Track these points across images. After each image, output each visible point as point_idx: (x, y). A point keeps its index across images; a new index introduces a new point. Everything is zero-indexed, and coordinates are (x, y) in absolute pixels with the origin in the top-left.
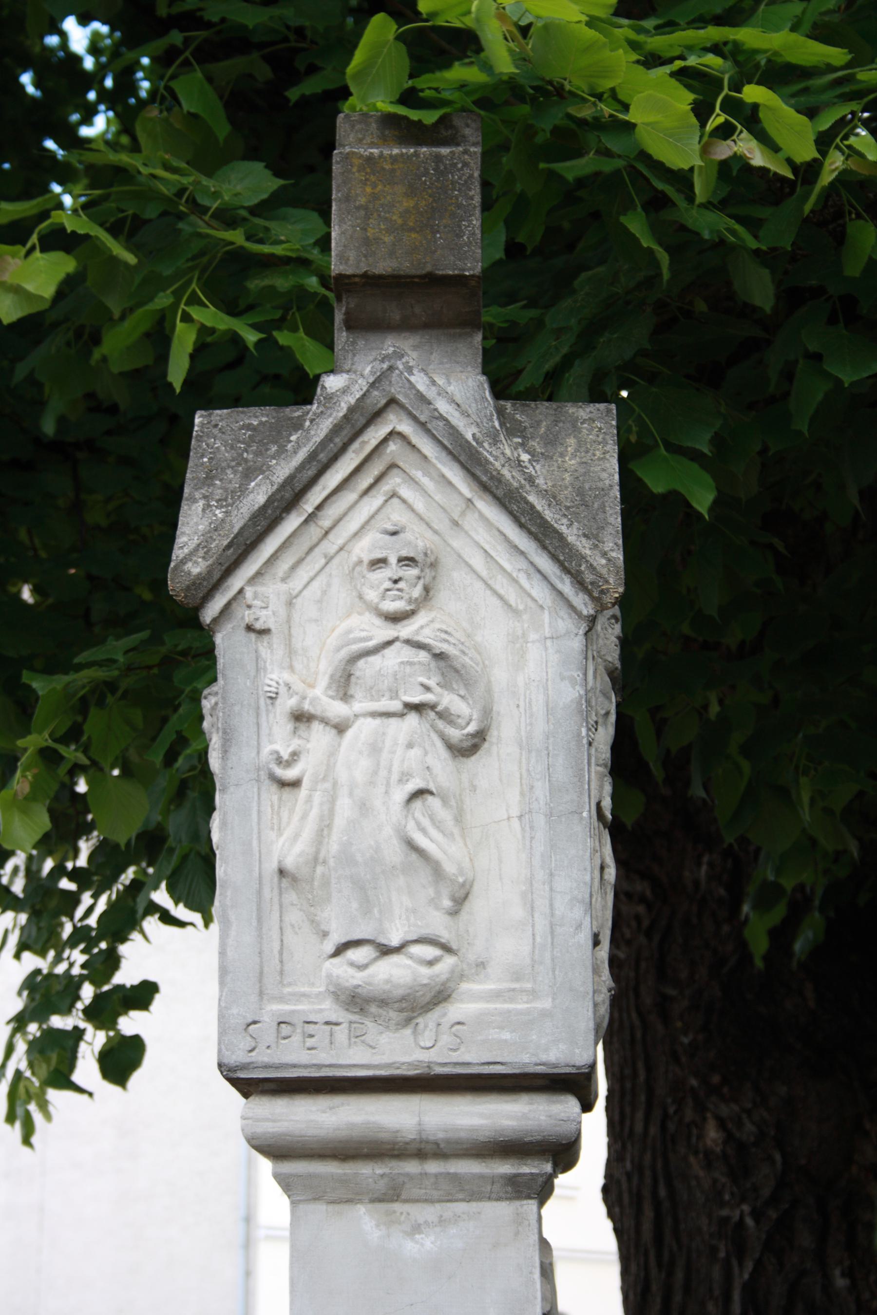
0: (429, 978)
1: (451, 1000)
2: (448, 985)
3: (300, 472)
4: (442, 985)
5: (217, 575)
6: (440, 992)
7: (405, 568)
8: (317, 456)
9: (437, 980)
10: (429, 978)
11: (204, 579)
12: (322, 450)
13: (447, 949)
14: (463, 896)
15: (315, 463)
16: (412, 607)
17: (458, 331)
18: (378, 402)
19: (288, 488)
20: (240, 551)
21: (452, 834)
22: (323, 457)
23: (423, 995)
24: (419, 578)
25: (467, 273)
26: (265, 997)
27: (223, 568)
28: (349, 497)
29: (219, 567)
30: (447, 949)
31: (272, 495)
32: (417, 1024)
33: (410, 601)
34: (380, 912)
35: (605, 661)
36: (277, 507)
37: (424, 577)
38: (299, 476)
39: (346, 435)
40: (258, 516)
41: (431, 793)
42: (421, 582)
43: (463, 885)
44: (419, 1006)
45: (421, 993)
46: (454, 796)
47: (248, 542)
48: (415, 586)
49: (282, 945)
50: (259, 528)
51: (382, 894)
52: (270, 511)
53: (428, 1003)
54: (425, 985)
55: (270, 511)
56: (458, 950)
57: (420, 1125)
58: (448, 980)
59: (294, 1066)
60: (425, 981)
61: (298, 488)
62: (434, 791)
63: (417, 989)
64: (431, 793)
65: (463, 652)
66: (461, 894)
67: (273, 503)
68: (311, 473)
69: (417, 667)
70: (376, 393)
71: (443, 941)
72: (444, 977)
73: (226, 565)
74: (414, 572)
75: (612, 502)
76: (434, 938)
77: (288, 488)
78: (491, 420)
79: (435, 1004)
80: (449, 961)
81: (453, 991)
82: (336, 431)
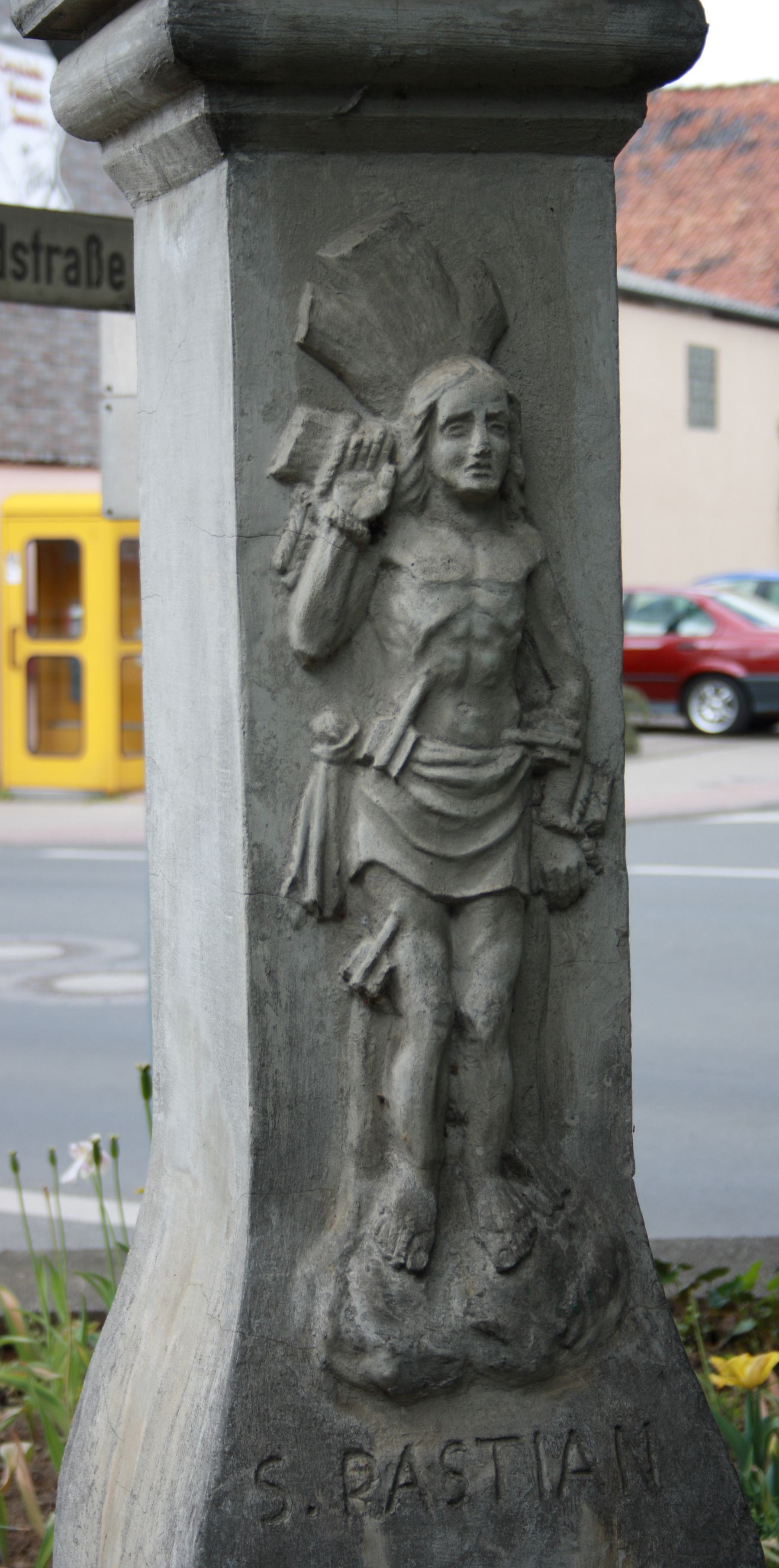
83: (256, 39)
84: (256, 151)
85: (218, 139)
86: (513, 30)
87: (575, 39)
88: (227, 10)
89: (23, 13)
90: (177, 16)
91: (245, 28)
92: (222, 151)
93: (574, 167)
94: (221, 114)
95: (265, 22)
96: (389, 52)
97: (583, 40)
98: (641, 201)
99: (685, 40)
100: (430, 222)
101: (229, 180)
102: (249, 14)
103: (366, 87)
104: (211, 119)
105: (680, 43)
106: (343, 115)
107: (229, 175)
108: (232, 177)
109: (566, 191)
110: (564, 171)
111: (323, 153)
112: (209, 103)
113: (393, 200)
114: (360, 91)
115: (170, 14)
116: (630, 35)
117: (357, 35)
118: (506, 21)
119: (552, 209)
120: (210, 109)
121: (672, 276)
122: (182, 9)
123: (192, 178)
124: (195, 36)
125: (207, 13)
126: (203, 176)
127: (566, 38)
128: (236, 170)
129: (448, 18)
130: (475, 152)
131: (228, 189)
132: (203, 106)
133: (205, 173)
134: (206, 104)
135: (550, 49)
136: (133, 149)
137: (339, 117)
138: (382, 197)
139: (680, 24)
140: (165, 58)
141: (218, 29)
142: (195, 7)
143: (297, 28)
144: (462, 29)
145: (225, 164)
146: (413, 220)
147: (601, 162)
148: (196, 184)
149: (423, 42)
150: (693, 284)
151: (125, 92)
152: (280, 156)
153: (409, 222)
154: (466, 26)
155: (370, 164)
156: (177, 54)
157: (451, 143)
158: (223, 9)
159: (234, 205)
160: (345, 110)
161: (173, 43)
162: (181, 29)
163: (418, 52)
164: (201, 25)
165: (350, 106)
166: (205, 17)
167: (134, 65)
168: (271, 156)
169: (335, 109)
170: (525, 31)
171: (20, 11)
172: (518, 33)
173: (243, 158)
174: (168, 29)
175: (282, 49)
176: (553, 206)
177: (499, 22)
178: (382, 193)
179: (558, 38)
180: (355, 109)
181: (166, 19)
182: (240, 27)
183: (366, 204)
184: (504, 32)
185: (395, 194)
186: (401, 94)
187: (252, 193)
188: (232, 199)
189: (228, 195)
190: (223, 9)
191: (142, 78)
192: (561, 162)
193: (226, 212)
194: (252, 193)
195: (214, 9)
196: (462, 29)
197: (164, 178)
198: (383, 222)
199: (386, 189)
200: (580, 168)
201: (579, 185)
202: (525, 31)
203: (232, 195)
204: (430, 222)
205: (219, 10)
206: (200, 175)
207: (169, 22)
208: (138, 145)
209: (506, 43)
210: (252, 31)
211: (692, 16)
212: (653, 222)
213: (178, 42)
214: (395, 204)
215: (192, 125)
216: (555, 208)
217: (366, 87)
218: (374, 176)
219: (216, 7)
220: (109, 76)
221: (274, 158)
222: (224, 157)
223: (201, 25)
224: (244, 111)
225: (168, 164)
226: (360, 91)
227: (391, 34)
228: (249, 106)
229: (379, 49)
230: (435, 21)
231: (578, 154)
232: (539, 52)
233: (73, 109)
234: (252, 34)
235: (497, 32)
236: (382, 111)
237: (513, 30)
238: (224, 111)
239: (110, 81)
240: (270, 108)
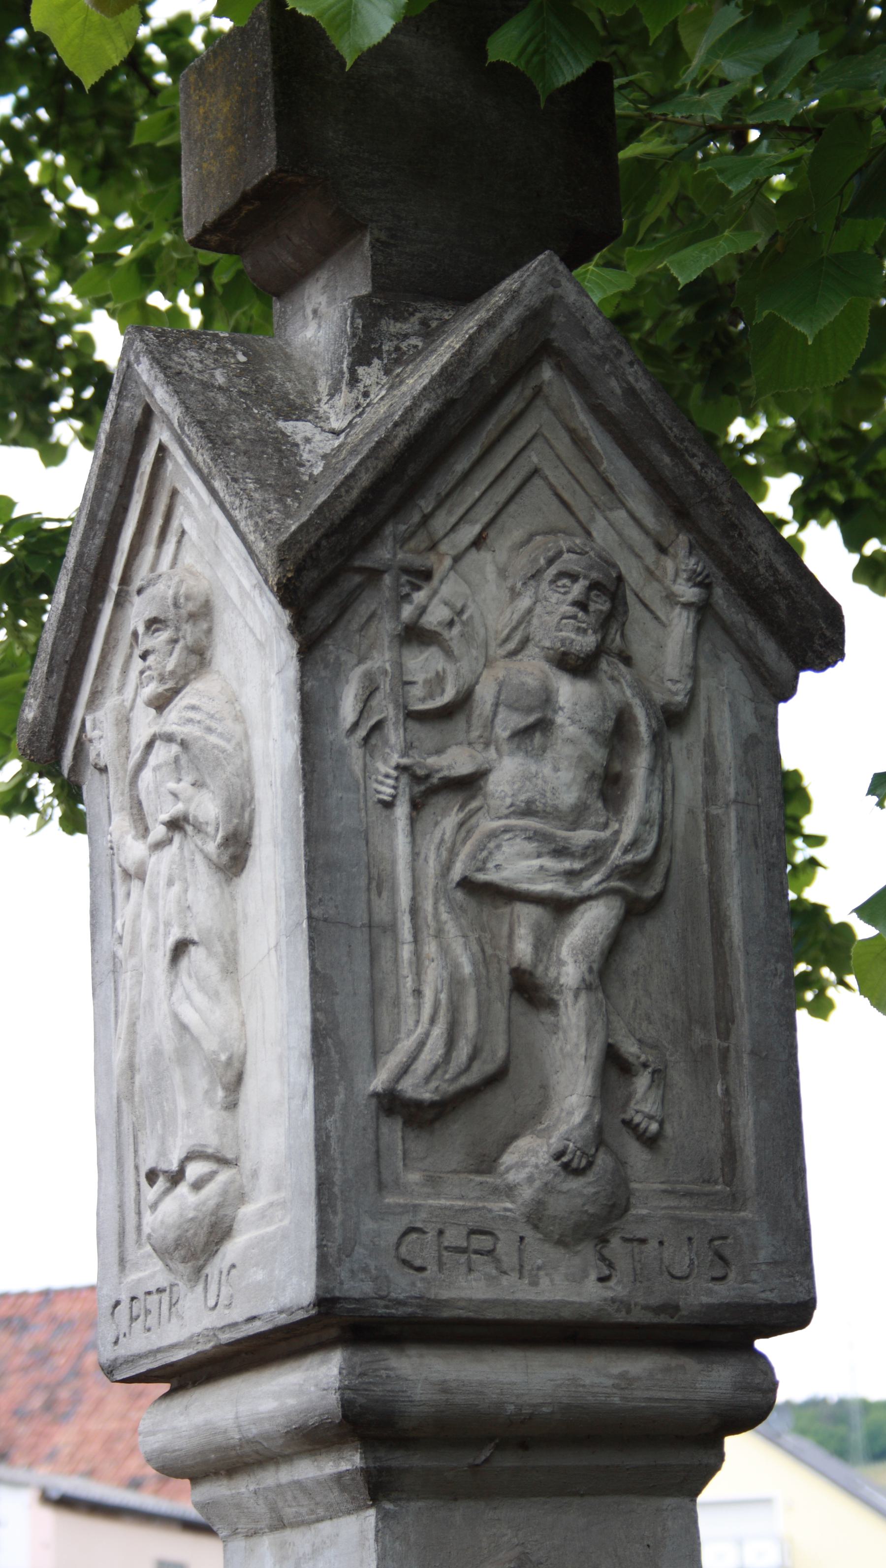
0: (195, 1210)
1: (234, 1233)
2: (221, 1213)
3: (86, 545)
4: (212, 1214)
5: (53, 713)
6: (213, 1226)
7: (156, 634)
8: (96, 515)
9: (204, 1209)
10: (195, 1210)
11: (42, 724)
12: (99, 507)
13: (222, 1161)
14: (233, 1079)
15: (98, 526)
16: (170, 684)
17: (352, 242)
18: (133, 415)
19: (81, 571)
20: (64, 673)
21: (217, 994)
22: (103, 514)
23: (195, 1234)
24: (175, 641)
25: (267, 174)
26: (128, 1265)
27: (56, 701)
28: (149, 551)
29: (51, 702)
30: (222, 1161)
31: (69, 587)
32: (207, 1276)
33: (162, 679)
34: (164, 1125)
35: (543, 648)
36: (80, 600)
37: (184, 638)
38: (86, 551)
39: (117, 474)
40: (64, 621)
41: (194, 943)
42: (178, 647)
43: (229, 1063)
44: (199, 1250)
45: (192, 1232)
46: (220, 937)
47: (68, 659)
48: (171, 655)
49: (139, 1190)
50: (72, 635)
51: (167, 1099)
52: (74, 610)
53: (207, 1244)
54: (192, 1219)
55: (74, 610)
56: (237, 1159)
57: (237, 1418)
58: (219, 1206)
59: (140, 1356)
60: (191, 1215)
61: (92, 567)
62: (196, 938)
63: (186, 1226)
64: (194, 943)
65: (209, 730)
66: (230, 1075)
67: (73, 597)
68: (98, 541)
69: (164, 769)
70: (127, 404)
71: (210, 1151)
72: (212, 1203)
73: (57, 696)
74: (164, 636)
75: (260, 458)
76: (200, 1149)
77: (81, 571)
78: (342, 362)
79: (217, 1243)
80: (224, 1176)
81: (233, 1219)
82: (105, 475)
83: (411, 1401)
84: (400, 1499)
85: (369, 1489)
86: (622, 1389)
87: (673, 1395)
88: (388, 1377)
89: (119, 1362)
90: (346, 1383)
91: (403, 1392)
92: (371, 1500)
93: (664, 1507)
94: (375, 1467)
95: (420, 1386)
96: (521, 1410)
97: (679, 1397)
98: (99, 1403)
99: (761, 1395)
100: (547, 1560)
101: (377, 1526)
102: (406, 1380)
103: (497, 1441)
104: (366, 1472)
105: (757, 1398)
106: (477, 1465)
107: (377, 1522)
108: (380, 1523)
109: (659, 1529)
110: (657, 1510)
111: (456, 1499)
112: (364, 1458)
113: (515, 1541)
114: (492, 1445)
115: (340, 1381)
116: (717, 1391)
117: (494, 1396)
118: (617, 1381)
119: (648, 1546)
120: (366, 1463)
121: (135, 1484)
122: (351, 1376)
123: (319, 1520)
124: (361, 1400)
125: (371, 1380)
126: (335, 1520)
127: (666, 1395)
128: (384, 1517)
129: (569, 1380)
130: (582, 1495)
131: (376, 1535)
132: (358, 1461)
133: (340, 1517)
134: (361, 1459)
135: (653, 1404)
136: (243, 1490)
137: (474, 1467)
138: (506, 1538)
139: (757, 1381)
140: (327, 1419)
141: (381, 1394)
142: (362, 1374)
143: (445, 1391)
144: (581, 1389)
145: (372, 1512)
146: (533, 1559)
147: (687, 1500)
148: (326, 1527)
149: (549, 1401)
150: (157, 1492)
151: (257, 1442)
152: (420, 1504)
153: (531, 1561)
154: (584, 1386)
155: (495, 1508)
156: (345, 1416)
157: (563, 1488)
158: (384, 1376)
159: (382, 1549)
160: (479, 1461)
161: (343, 1406)
162: (349, 1394)
163: (544, 1409)
164: (366, 1390)
165: (483, 1458)
166: (370, 1383)
167: (281, 1420)
168: (412, 1503)
169: (471, 1461)
170: (632, 1389)
171: (116, 1359)
172: (626, 1391)
173: (389, 1506)
174: (338, 1394)
175: (433, 1410)
176: (649, 1543)
177: (610, 1382)
178: (506, 1535)
179: (659, 1395)
180: (487, 1460)
181: (337, 1385)
182: (399, 1391)
183: (493, 1545)
184: (615, 1391)
185: (516, 1536)
186: (524, 1445)
187: (397, 1538)
188: (380, 1544)
189: (376, 1540)
190: (384, 1376)
191: (287, 1432)
192: (654, 1503)
193: (374, 1556)
194: (397, 1538)
195: (377, 1376)
196: (581, 1389)
197: (281, 1519)
198: (511, 1561)
199: (509, 1531)
200: (670, 1508)
201: (670, 1523)
202: (632, 1389)
203: (380, 1540)
204: (547, 1560)
205: (381, 1376)
206: (331, 1519)
207: (339, 1388)
208: (252, 1488)
209: (616, 1400)
210: (408, 1394)
211: (766, 1374)
212: (113, 1425)
213: (346, 1405)
214: (517, 1545)
215: (339, 1478)
216: (651, 1545)
217: (497, 1441)
218: (499, 1519)
219: (378, 1374)
220: (239, 1426)
221: (414, 1506)
222: (372, 1506)
223: (366, 1390)
224: (394, 1464)
225: (289, 1506)
226: (492, 1445)
227: (523, 1394)
228: (397, 1459)
229: (512, 1407)
230: (559, 1382)
231: (667, 1495)
232: (644, 1407)
233: (175, 1451)
234: (408, 1397)
235: (609, 1391)
236: (509, 1460)
237: (622, 1389)
238: (377, 1464)
239: (240, 1431)
240: (416, 1460)
